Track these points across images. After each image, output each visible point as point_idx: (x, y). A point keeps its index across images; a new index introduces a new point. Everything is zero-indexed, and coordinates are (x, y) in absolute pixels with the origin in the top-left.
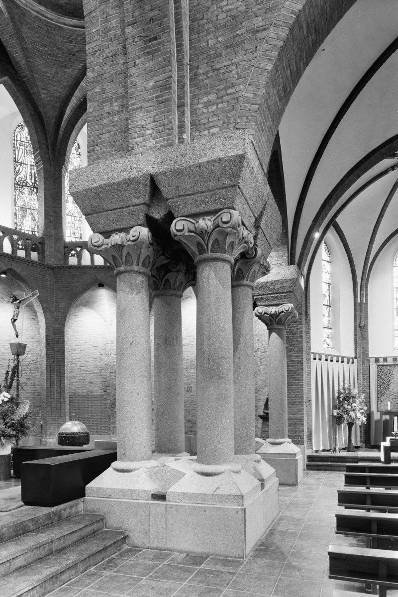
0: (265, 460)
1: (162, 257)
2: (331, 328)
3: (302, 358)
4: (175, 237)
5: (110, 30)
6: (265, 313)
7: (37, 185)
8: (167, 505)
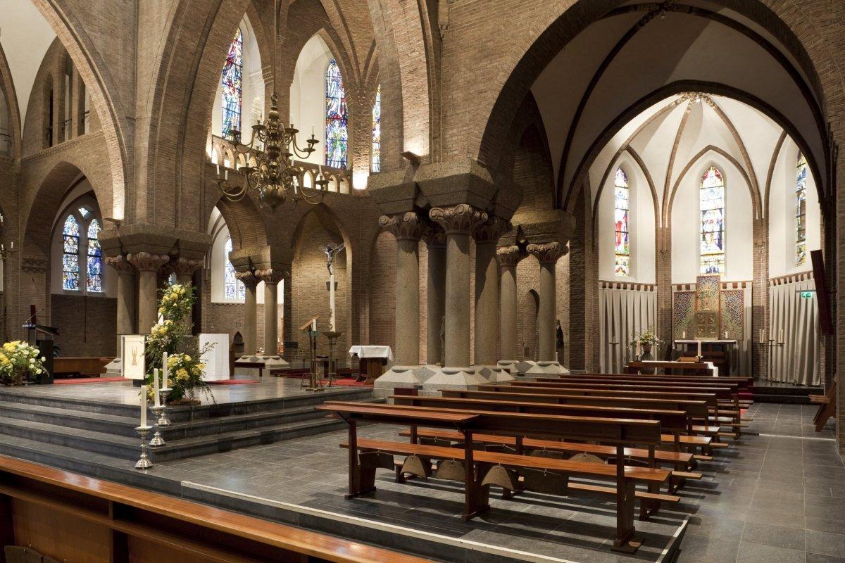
2: (628, 255)
5: (395, 83)
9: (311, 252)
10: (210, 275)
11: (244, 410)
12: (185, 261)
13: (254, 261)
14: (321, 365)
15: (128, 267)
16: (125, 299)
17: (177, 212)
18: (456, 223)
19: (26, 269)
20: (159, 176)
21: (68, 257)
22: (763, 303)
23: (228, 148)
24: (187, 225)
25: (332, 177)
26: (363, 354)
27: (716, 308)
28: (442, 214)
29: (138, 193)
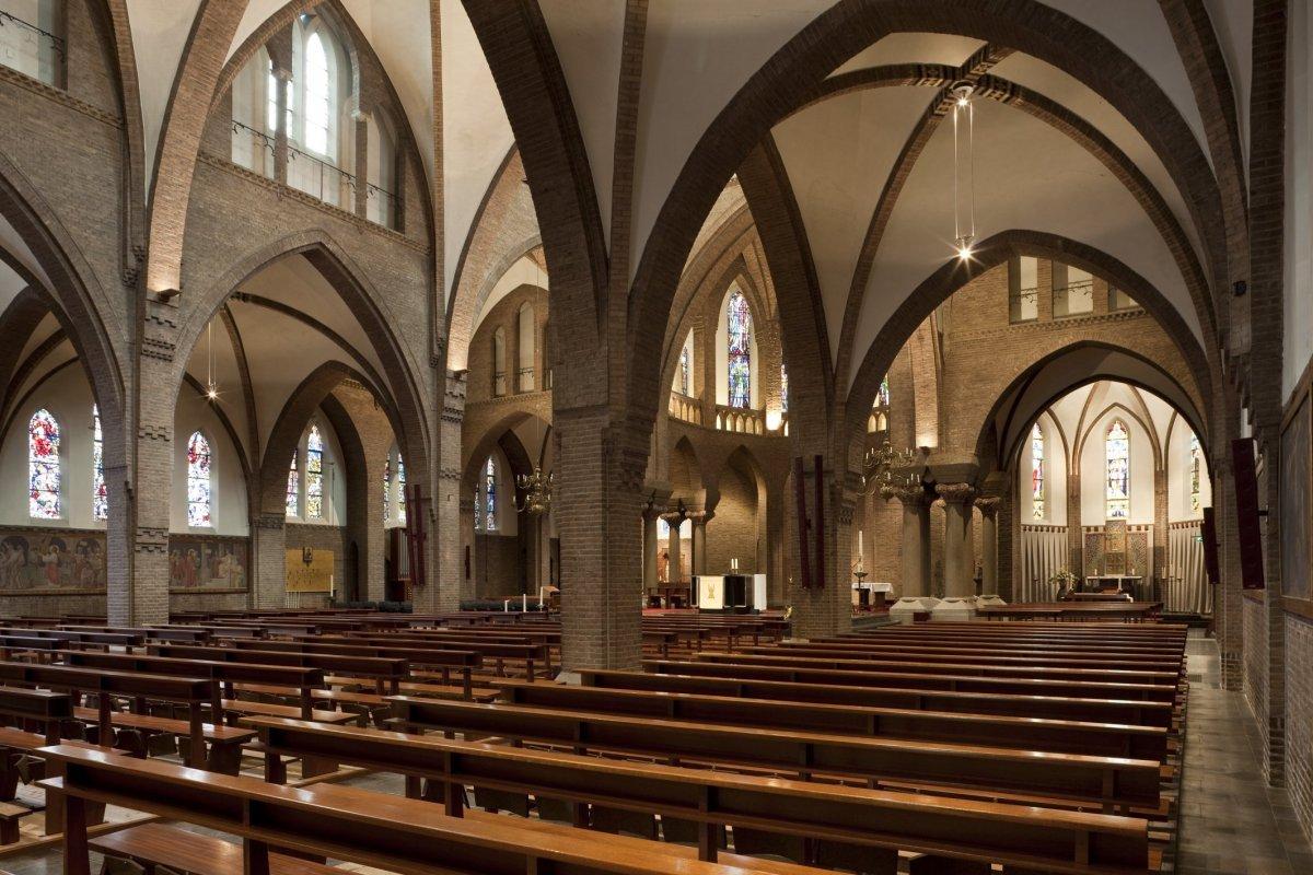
13: (684, 502)
22: (1163, 544)
27: (1123, 551)
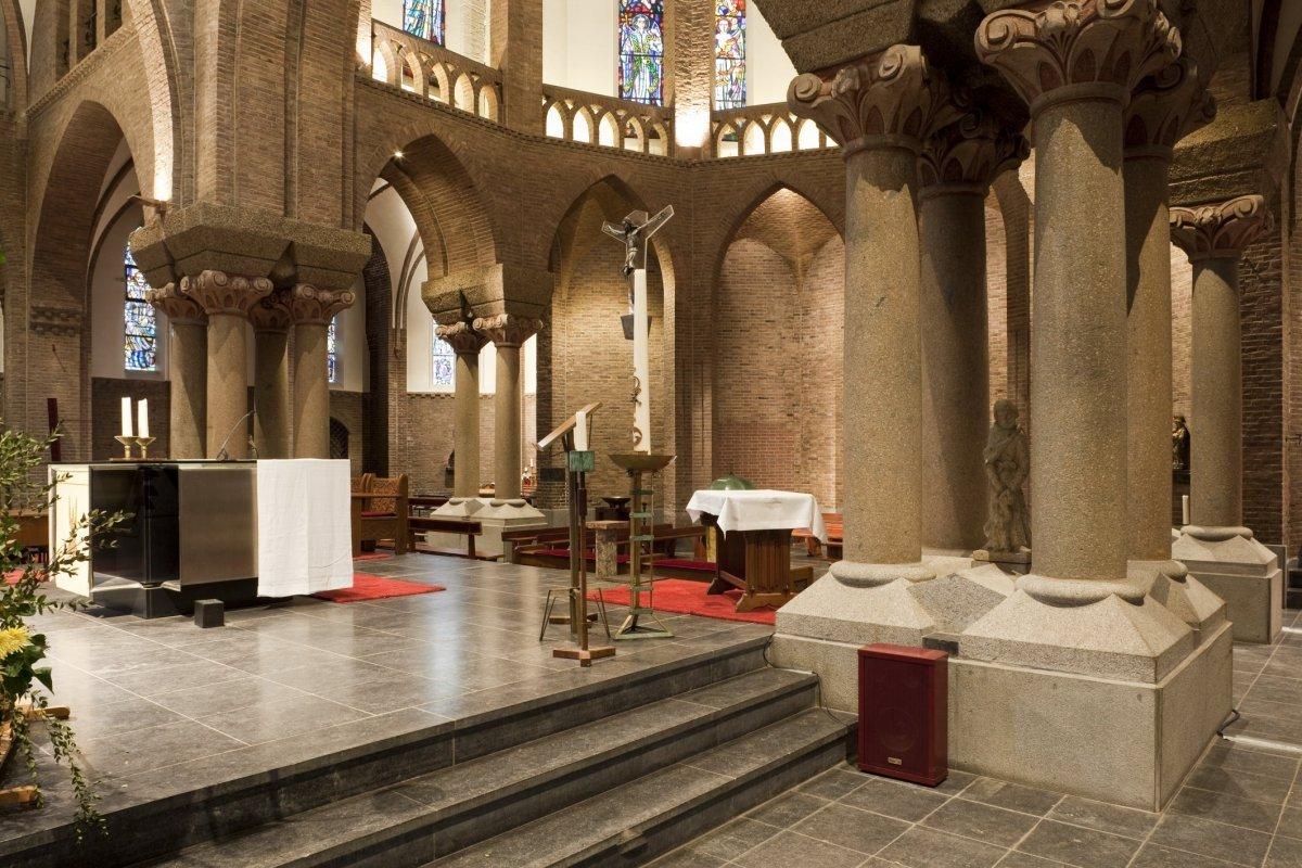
0: (1200, 579)
1: (950, 109)
3: (1281, 330)
4: (984, 57)
6: (1184, 223)
7: (661, 7)
8: (960, 665)
9: (590, 285)
10: (404, 341)
11: (263, 808)
12: (309, 292)
13: (472, 298)
14: (609, 539)
15: (191, 309)
16: (185, 379)
17: (288, 182)
18: (1087, 56)
19: (39, 329)
20: (244, 95)
21: (134, 307)
23: (408, 51)
24: (313, 210)
25: (633, 122)
26: (735, 519)
28: (1028, 30)
29: (202, 138)
